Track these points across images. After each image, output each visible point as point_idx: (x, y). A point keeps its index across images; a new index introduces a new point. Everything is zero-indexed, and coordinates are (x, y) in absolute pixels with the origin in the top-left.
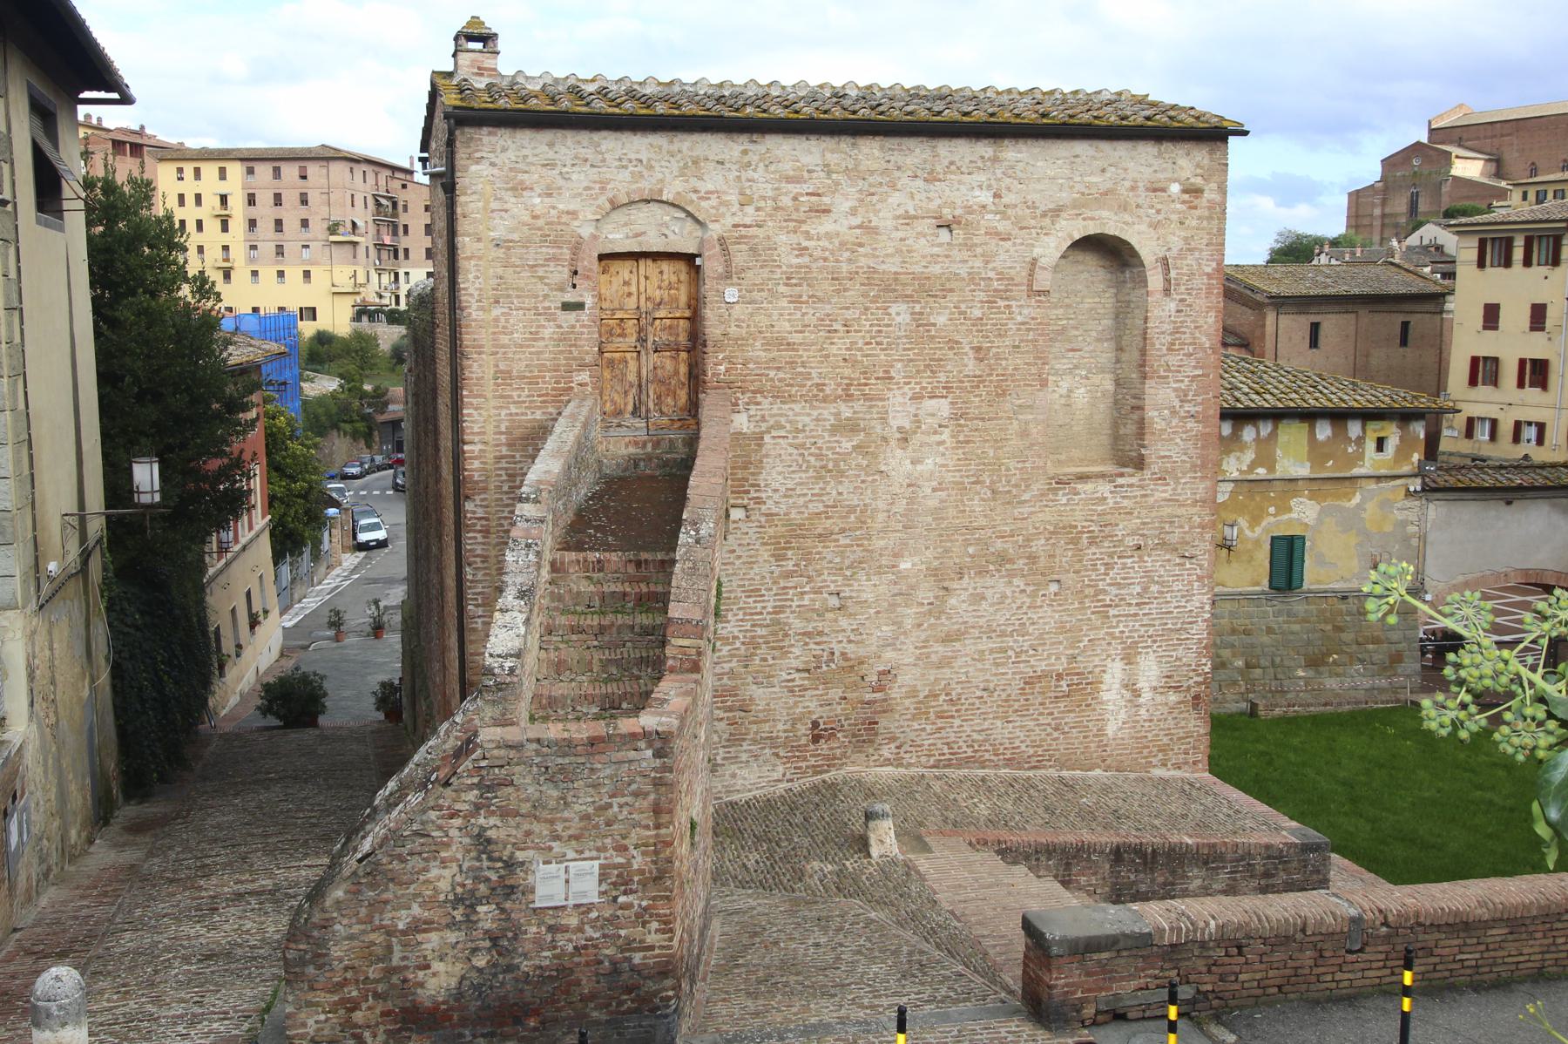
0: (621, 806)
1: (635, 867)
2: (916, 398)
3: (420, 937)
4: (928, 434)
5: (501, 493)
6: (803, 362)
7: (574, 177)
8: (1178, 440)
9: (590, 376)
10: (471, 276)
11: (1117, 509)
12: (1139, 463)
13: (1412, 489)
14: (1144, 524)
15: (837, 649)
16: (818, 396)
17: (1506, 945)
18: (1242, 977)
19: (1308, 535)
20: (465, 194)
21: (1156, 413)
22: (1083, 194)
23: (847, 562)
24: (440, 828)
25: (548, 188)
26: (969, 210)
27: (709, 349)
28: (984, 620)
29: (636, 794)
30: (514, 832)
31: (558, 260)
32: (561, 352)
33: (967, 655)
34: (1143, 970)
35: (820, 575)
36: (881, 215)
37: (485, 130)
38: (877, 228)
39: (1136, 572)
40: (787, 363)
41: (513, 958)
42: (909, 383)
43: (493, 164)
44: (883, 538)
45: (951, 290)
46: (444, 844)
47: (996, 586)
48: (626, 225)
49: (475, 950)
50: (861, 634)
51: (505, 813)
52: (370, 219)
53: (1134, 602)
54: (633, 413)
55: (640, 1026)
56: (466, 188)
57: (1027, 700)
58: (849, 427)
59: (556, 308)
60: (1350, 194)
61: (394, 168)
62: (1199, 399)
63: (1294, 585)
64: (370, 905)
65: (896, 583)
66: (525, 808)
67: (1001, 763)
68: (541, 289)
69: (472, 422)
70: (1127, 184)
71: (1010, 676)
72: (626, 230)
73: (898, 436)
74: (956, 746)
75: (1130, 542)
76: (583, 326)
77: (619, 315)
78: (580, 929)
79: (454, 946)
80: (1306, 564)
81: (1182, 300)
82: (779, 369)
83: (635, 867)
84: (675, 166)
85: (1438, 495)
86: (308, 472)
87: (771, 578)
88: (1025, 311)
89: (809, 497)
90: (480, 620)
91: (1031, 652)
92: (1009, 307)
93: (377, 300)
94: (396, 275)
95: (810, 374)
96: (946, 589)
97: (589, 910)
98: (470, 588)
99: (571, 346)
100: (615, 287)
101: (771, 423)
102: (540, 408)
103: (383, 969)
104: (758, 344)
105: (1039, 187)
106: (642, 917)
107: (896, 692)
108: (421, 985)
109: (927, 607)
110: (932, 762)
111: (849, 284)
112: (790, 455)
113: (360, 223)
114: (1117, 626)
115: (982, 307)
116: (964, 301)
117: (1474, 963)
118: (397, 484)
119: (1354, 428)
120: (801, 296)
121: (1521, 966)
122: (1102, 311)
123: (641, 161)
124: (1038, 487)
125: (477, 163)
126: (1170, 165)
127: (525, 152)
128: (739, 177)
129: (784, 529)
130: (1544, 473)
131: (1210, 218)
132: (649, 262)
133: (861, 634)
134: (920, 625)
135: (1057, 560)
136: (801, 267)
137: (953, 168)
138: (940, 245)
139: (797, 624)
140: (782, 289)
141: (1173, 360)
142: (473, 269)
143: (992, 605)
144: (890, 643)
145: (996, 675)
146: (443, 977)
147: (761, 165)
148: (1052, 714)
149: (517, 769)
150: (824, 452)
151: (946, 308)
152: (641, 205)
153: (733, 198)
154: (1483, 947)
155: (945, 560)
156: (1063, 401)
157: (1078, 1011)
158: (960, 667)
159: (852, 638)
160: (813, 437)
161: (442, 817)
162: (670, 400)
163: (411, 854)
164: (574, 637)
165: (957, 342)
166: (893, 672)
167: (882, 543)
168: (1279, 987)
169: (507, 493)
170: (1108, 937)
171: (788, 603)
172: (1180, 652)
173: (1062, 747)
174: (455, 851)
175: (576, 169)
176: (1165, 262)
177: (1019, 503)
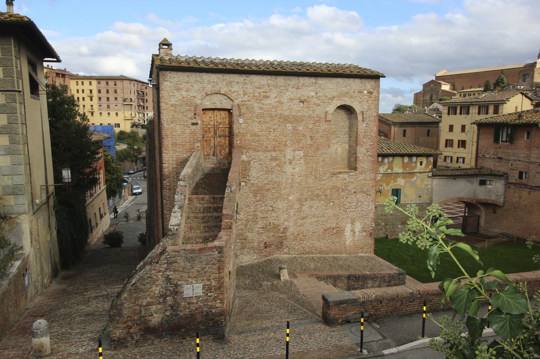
0: (209, 268)
1: (213, 285)
3: (150, 307)
4: (297, 161)
7: (195, 86)
10: (164, 115)
11: (349, 182)
12: (355, 169)
15: (272, 222)
16: (266, 150)
18: (381, 310)
19: (402, 188)
21: (360, 155)
23: (274, 197)
24: (156, 275)
26: (308, 97)
27: (235, 136)
29: (213, 264)
30: (177, 276)
32: (191, 137)
34: (355, 309)
37: (168, 72)
38: (282, 102)
43: (171, 82)
45: (304, 120)
47: (316, 203)
48: (210, 100)
49: (166, 310)
51: (175, 271)
62: (372, 151)
66: (181, 269)
68: (185, 119)
70: (352, 91)
73: (289, 161)
75: (353, 191)
77: (208, 127)
78: (197, 303)
79: (160, 309)
81: (367, 123)
82: (255, 142)
83: (213, 285)
84: (224, 83)
88: (324, 126)
92: (320, 125)
93: (138, 122)
94: (144, 114)
96: (302, 204)
97: (200, 298)
100: (207, 118)
103: (139, 317)
104: (249, 135)
106: (215, 299)
107: (288, 234)
108: (150, 321)
109: (297, 210)
111: (275, 118)
113: (133, 99)
119: (414, 159)
125: (166, 82)
132: (217, 111)
134: (295, 215)
138: (300, 107)
140: (256, 119)
141: (365, 140)
143: (315, 209)
146: (157, 318)
147: (249, 84)
149: (178, 258)
151: (302, 125)
152: (215, 95)
153: (241, 93)
156: (335, 151)
157: (337, 321)
161: (156, 272)
162: (223, 151)
163: (147, 283)
164: (195, 220)
165: (305, 135)
167: (284, 192)
175: (196, 84)
176: (362, 112)
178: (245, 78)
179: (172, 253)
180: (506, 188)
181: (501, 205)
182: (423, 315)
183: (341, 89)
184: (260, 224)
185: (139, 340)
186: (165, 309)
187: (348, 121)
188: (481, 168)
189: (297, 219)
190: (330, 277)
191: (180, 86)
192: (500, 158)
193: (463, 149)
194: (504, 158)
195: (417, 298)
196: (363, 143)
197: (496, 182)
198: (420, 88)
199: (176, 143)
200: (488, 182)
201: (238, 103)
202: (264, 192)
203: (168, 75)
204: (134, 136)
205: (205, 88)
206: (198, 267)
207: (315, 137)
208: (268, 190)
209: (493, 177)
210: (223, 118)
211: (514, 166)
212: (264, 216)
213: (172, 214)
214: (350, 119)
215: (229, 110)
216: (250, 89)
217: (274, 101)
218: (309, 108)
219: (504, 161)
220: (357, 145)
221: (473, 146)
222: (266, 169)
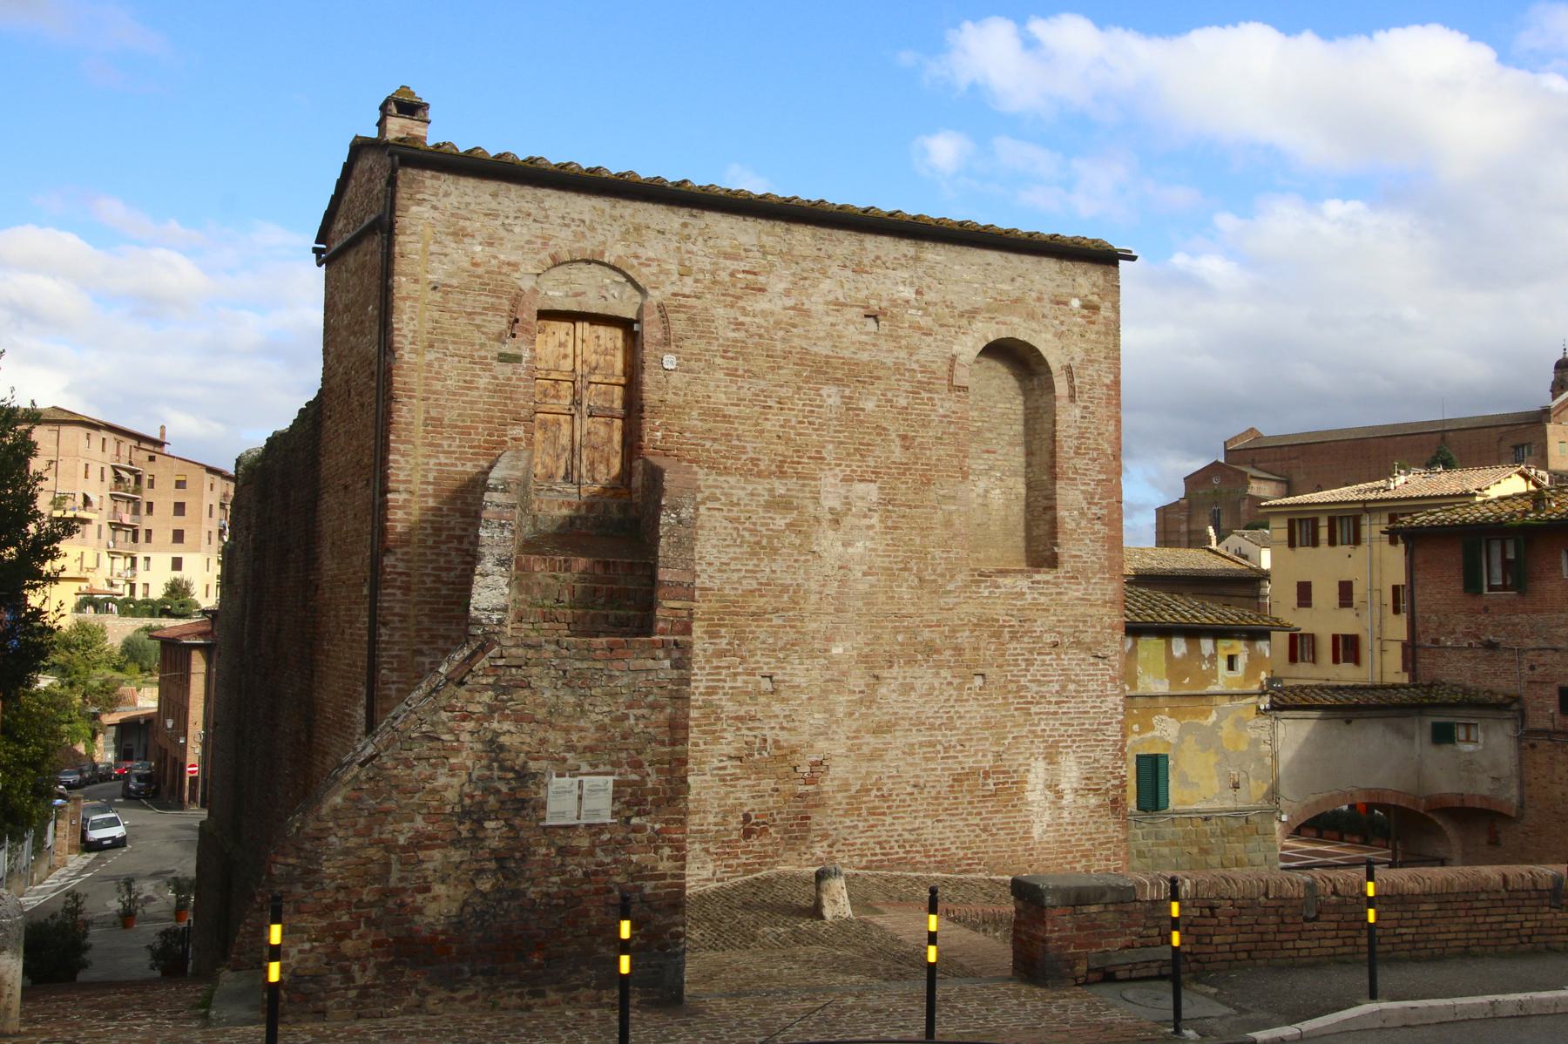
0: (637, 718)
1: (650, 785)
2: (846, 481)
3: (421, 854)
4: (858, 517)
5: (426, 547)
6: (738, 436)
7: (517, 230)
8: (1087, 541)
9: (525, 432)
10: (405, 317)
11: (1035, 605)
12: (1052, 562)
13: (1262, 707)
14: (1060, 621)
15: (770, 735)
16: (752, 471)
17: (1434, 921)
18: (1217, 939)
19: (1170, 753)
20: (404, 234)
21: (1066, 513)
22: (996, 299)
23: (780, 644)
24: (451, 731)
25: (490, 238)
26: (894, 303)
27: (646, 414)
28: (914, 711)
29: (652, 707)
30: (528, 740)
31: (497, 309)
32: (496, 404)
33: (897, 748)
34: (1129, 927)
35: (753, 656)
36: (813, 299)
37: (428, 173)
38: (808, 311)
39: (1055, 670)
40: (722, 434)
41: (519, 883)
42: (840, 465)
43: (434, 208)
44: (815, 621)
45: (879, 378)
46: (453, 749)
47: (924, 676)
48: (566, 283)
49: (480, 872)
50: (793, 721)
51: (519, 718)
52: (107, 494)
53: (1053, 700)
54: (564, 478)
55: (650, 966)
56: (405, 228)
57: (956, 798)
58: (780, 504)
59: (493, 358)
60: (1158, 510)
61: (140, 438)
62: (1104, 503)
63: (1161, 805)
64: (371, 815)
65: (828, 669)
66: (541, 714)
67: (932, 865)
68: (478, 338)
69: (398, 469)
70: (1034, 295)
71: (939, 772)
72: (566, 288)
73: (829, 516)
74: (887, 846)
75: (1049, 638)
76: (520, 379)
77: (554, 375)
78: (591, 853)
79: (458, 866)
80: (1170, 784)
81: (1085, 407)
82: (714, 440)
83: (650, 785)
84: (617, 230)
85: (1286, 713)
86: (44, 736)
87: (704, 656)
88: (947, 405)
89: (743, 573)
90: (394, 687)
91: (959, 748)
92: (931, 399)
93: (107, 588)
94: (134, 560)
95: (744, 447)
96: (877, 677)
97: (601, 832)
98: (385, 649)
99: (506, 398)
100: (550, 348)
101: (707, 494)
102: (471, 460)
103: (378, 890)
104: (695, 413)
105: (957, 289)
106: (654, 843)
107: (828, 786)
108: (419, 911)
109: (858, 696)
110: (864, 863)
111: (783, 362)
112: (725, 528)
113: (94, 498)
114: (1038, 725)
115: (907, 397)
116: (890, 390)
117: (1411, 938)
118: (130, 790)
119: (1207, 645)
120: (737, 370)
121: (1450, 944)
122: (1013, 417)
123: (584, 222)
124: (961, 578)
125: (418, 205)
126: (1070, 282)
127: (467, 199)
128: (679, 248)
129: (718, 605)
130: (1377, 694)
131: (1106, 334)
132: (586, 325)
133: (793, 721)
134: (851, 714)
135: (981, 653)
136: (737, 341)
137: (879, 262)
138: (868, 334)
139: (730, 707)
140: (718, 361)
141: (1080, 463)
142: (408, 310)
143: (921, 696)
144: (822, 732)
145: (925, 770)
146: (444, 902)
147: (700, 239)
148: (980, 814)
149: (535, 671)
150: (759, 528)
151: (874, 394)
152: (582, 265)
153: (673, 267)
154: (1417, 922)
155: (876, 647)
156: (980, 500)
157: (1072, 968)
158: (891, 761)
159: (785, 724)
160: (748, 512)
161: (454, 719)
162: (602, 468)
163: (419, 759)
164: (546, 625)
165: (884, 429)
166: (825, 763)
167: (814, 625)
168: (1249, 952)
169: (431, 547)
170: (1095, 888)
171: (721, 684)
172: (1098, 754)
173: (990, 850)
174: (464, 759)
175: (519, 222)
176: (1069, 370)
177: (945, 593)
178: (687, 219)
179: (514, 651)
180: (1521, 750)
181: (1513, 814)
182: (1376, 888)
183: (998, 286)
184: (730, 741)
185: (374, 986)
186: (475, 866)
187: (1020, 400)
188: (1431, 686)
189: (857, 731)
190: (994, 921)
191: (468, 223)
192: (1491, 646)
193: (1350, 665)
194: (1503, 645)
195: (1329, 905)
196: (1076, 472)
197: (1485, 731)
198: (1177, 492)
199: (441, 420)
200: (1461, 733)
201: (660, 299)
202: (742, 621)
203: (428, 182)
204: (85, 642)
205: (551, 237)
206: (600, 712)
207: (919, 440)
208: (757, 616)
209: (1474, 712)
210: (606, 353)
211: (1540, 670)
212: (742, 713)
213: (477, 578)
214: (1027, 393)
215: (628, 327)
216: (701, 258)
217: (779, 303)
218: (896, 339)
219: (1506, 655)
220: (1054, 478)
221: (1386, 657)
222: (752, 539)
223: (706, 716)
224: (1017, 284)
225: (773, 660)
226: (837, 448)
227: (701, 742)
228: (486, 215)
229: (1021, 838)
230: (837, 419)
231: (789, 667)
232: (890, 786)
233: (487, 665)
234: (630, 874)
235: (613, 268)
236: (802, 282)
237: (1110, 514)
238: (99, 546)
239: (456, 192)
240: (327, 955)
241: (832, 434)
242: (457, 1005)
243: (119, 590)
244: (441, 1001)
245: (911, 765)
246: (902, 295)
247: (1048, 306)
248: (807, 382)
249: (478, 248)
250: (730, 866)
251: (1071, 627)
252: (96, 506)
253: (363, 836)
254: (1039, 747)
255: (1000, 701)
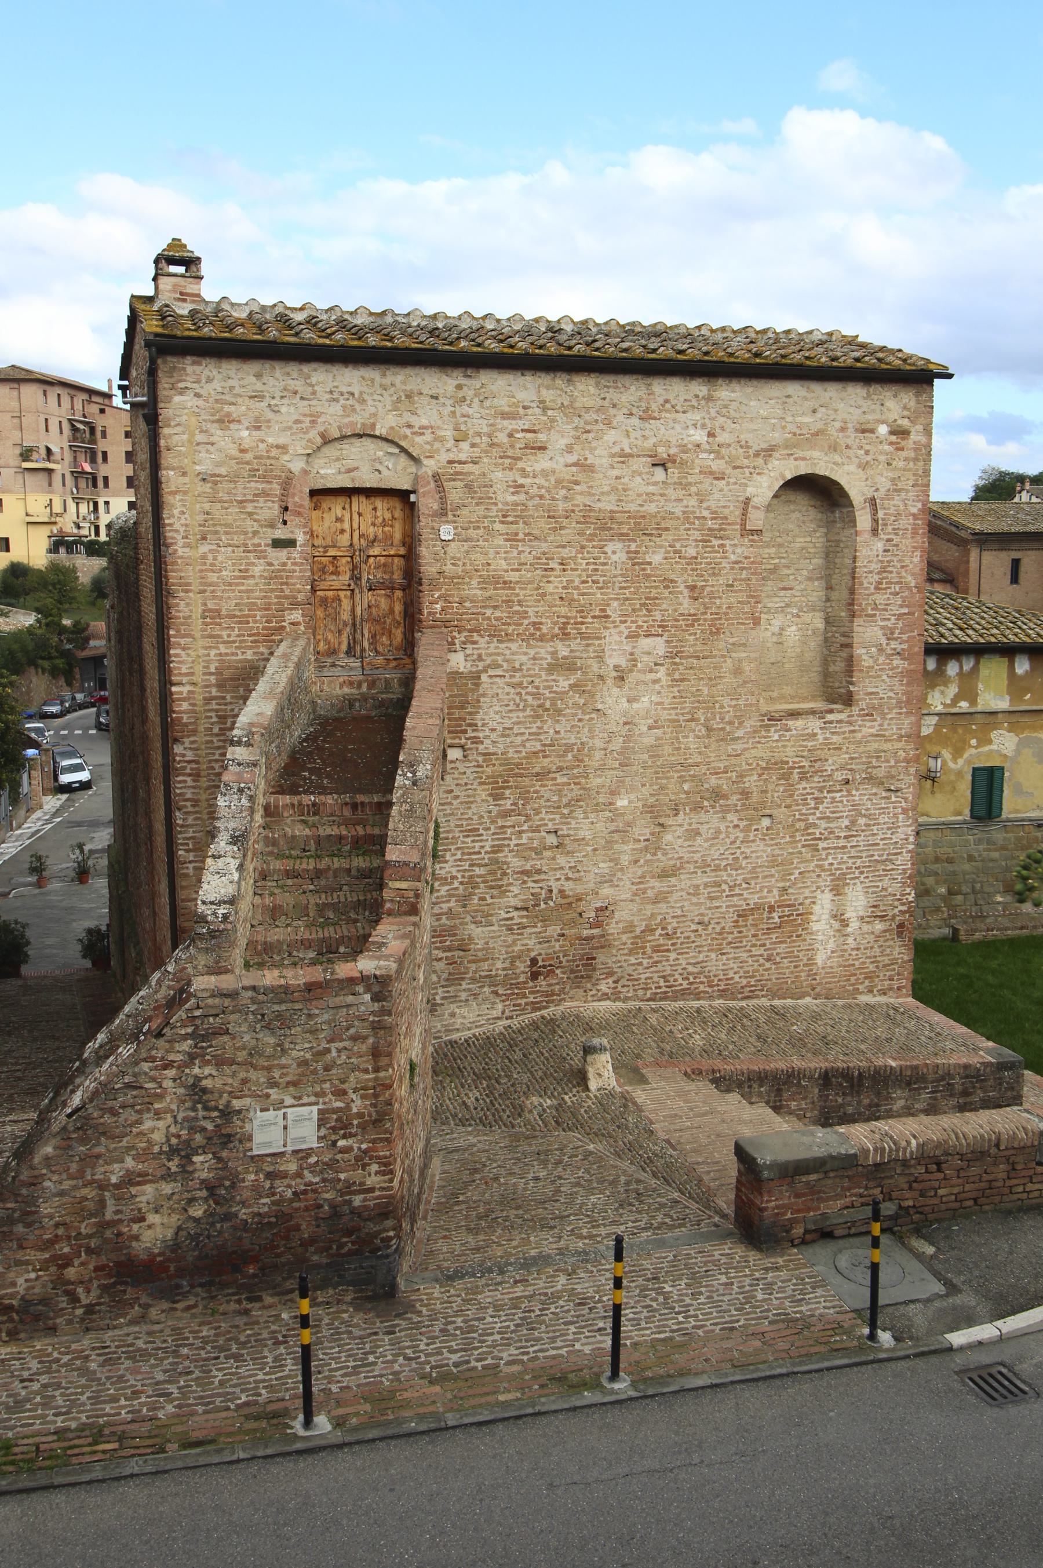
0: (339, 1051)
1: (355, 1110)
3: (134, 1190)
4: (644, 672)
5: (212, 735)
6: (519, 601)
7: (284, 409)
8: (885, 677)
10: (176, 512)
11: (827, 744)
12: (848, 700)
14: (852, 759)
15: (555, 886)
16: (535, 635)
18: (941, 1192)
19: (1006, 765)
20: (169, 426)
21: (864, 651)
22: (795, 434)
23: (565, 800)
24: (153, 1079)
27: (425, 587)
29: (354, 1039)
31: (268, 495)
32: (272, 591)
33: (682, 890)
34: (849, 1189)
35: (537, 814)
36: (597, 452)
37: (189, 360)
38: (592, 466)
43: (197, 395)
44: (600, 776)
45: (667, 529)
46: (156, 1095)
47: (710, 821)
48: (338, 459)
49: (191, 1201)
51: (220, 1062)
53: (842, 834)
54: (347, 653)
56: (169, 419)
58: (567, 666)
59: (267, 545)
61: (91, 392)
62: (905, 637)
64: (81, 1160)
65: (612, 821)
68: (250, 525)
69: (180, 662)
70: (838, 425)
71: (724, 910)
72: (338, 465)
75: (839, 776)
77: (332, 552)
78: (299, 1175)
79: (170, 1197)
81: (889, 540)
82: (495, 607)
83: (355, 1110)
84: (388, 400)
87: (489, 817)
88: (739, 550)
89: (527, 736)
90: (191, 866)
91: (744, 886)
92: (722, 546)
93: (75, 531)
94: (96, 504)
96: (662, 825)
97: (309, 1155)
98: (180, 832)
99: (282, 584)
100: (327, 524)
102: (250, 648)
103: (95, 1224)
106: (362, 1161)
107: (613, 928)
109: (643, 844)
111: (565, 522)
112: (508, 694)
113: (55, 449)
118: (101, 723)
120: (517, 534)
123: (353, 394)
124: (750, 724)
125: (181, 394)
126: (878, 407)
128: (454, 413)
132: (363, 499)
134: (636, 862)
136: (517, 505)
137: (668, 406)
138: (655, 484)
139: (516, 863)
140: (498, 526)
141: (880, 599)
144: (607, 880)
146: (159, 1229)
147: (476, 400)
148: (764, 945)
151: (661, 547)
152: (354, 440)
153: (448, 433)
156: (775, 639)
157: (787, 1232)
158: (676, 902)
159: (570, 875)
160: (530, 676)
161: (156, 1068)
163: (123, 1107)
164: (290, 882)
165: (672, 581)
166: (610, 908)
168: (975, 1200)
169: (217, 735)
171: (506, 842)
172: (886, 882)
174: (169, 1102)
175: (285, 401)
176: (873, 502)
177: (732, 739)
178: (462, 380)
179: (210, 1001)
183: (798, 419)
184: (516, 894)
186: (186, 1195)
189: (643, 877)
191: (233, 408)
196: (876, 608)
199: (219, 611)
201: (435, 468)
203: (190, 369)
205: (320, 414)
207: (708, 589)
208: (541, 776)
212: (528, 868)
213: (209, 861)
217: (562, 460)
218: (685, 486)
222: (535, 703)
223: (492, 873)
224: (819, 415)
225: (558, 817)
226: (622, 605)
227: (488, 897)
228: (251, 397)
229: (805, 965)
230: (622, 575)
231: (573, 822)
232: (675, 925)
233: (184, 1016)
234: (338, 1191)
235: (386, 440)
236: (585, 436)
237: (910, 647)
238: (64, 493)
239: (220, 376)
240: (52, 1282)
241: (617, 591)
242: (179, 1314)
243: (85, 532)
244: (163, 1311)
245: (696, 904)
246: (692, 439)
247: (853, 436)
248: (591, 541)
249: (245, 433)
250: (519, 1005)
251: (863, 763)
252: (58, 457)
253: (76, 1178)
254: (826, 880)
255: (788, 839)
